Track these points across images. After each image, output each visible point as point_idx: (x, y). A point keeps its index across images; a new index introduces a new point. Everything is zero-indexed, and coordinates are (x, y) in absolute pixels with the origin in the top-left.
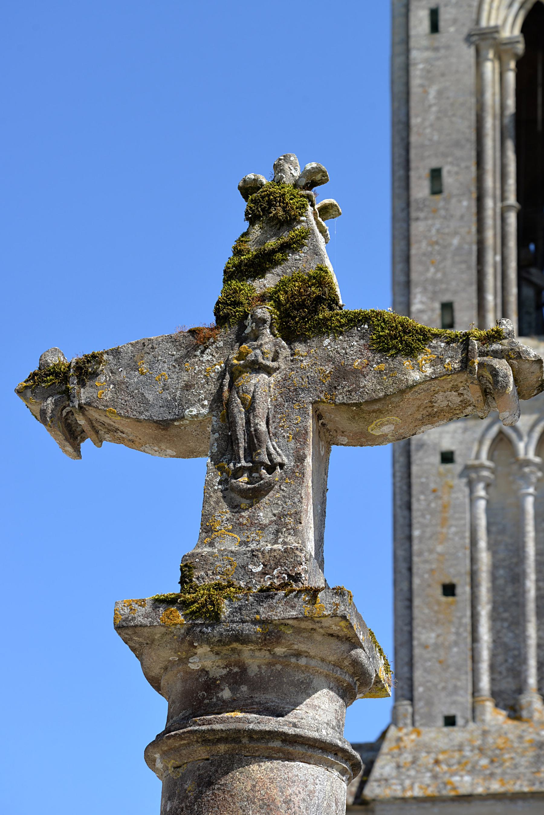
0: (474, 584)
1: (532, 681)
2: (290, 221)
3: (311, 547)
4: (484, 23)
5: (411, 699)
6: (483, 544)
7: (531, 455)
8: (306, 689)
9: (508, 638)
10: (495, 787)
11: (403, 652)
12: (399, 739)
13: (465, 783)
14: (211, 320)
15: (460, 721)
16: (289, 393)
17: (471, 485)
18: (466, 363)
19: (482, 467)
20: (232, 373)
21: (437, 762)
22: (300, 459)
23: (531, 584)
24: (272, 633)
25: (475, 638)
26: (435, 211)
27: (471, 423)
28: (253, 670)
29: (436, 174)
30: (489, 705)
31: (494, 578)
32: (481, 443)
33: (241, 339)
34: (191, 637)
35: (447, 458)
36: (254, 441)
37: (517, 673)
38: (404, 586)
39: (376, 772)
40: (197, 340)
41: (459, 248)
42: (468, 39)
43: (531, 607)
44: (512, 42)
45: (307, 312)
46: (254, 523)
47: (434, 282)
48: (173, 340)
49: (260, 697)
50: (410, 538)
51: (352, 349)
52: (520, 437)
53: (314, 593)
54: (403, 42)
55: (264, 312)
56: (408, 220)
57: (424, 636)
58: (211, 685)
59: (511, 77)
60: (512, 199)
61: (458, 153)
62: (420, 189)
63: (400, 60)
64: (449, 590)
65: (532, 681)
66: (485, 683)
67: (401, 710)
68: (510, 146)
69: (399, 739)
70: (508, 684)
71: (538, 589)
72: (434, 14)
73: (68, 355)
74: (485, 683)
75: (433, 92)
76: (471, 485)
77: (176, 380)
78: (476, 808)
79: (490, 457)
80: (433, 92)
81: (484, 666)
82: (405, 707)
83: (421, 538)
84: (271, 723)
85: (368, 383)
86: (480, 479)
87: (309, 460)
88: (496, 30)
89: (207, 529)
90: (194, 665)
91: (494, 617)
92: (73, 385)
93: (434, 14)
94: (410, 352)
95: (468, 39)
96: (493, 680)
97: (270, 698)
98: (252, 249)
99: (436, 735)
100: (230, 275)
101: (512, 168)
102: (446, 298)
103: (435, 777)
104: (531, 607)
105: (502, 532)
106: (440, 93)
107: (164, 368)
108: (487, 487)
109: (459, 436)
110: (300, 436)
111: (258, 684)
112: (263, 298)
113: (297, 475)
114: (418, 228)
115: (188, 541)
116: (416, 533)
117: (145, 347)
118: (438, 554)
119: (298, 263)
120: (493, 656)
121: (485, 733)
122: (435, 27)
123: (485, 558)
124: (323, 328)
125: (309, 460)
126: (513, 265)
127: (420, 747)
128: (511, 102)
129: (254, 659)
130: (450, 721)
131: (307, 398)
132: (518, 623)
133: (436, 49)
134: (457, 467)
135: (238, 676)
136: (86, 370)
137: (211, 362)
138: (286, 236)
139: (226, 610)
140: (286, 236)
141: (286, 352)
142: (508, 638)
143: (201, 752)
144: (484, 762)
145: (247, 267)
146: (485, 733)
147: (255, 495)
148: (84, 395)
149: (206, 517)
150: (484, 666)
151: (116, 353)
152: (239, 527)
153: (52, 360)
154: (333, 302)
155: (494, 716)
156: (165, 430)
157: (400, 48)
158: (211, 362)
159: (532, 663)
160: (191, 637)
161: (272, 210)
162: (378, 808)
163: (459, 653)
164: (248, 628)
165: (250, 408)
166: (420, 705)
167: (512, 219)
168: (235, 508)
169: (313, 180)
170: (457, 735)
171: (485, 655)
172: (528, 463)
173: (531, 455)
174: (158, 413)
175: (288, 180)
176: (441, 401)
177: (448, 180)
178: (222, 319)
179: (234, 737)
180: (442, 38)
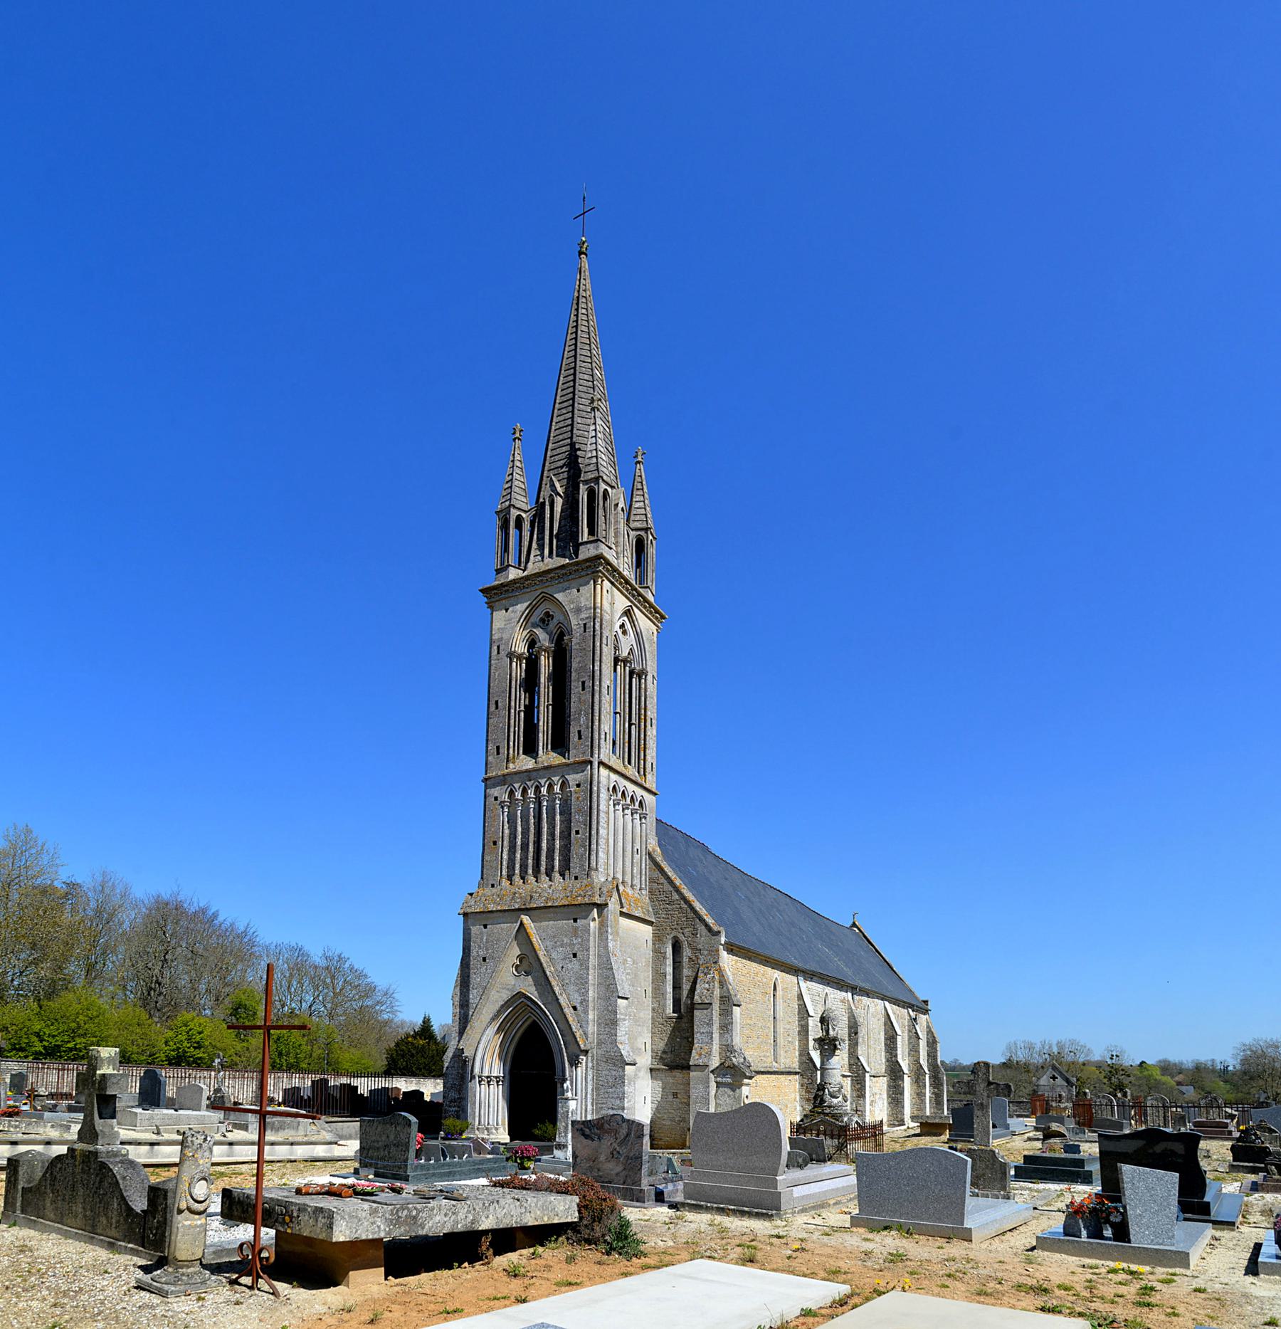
13: (492, 907)
29: (497, 702)
35: (496, 799)
64: (495, 843)
155: (505, 883)
170: (494, 890)
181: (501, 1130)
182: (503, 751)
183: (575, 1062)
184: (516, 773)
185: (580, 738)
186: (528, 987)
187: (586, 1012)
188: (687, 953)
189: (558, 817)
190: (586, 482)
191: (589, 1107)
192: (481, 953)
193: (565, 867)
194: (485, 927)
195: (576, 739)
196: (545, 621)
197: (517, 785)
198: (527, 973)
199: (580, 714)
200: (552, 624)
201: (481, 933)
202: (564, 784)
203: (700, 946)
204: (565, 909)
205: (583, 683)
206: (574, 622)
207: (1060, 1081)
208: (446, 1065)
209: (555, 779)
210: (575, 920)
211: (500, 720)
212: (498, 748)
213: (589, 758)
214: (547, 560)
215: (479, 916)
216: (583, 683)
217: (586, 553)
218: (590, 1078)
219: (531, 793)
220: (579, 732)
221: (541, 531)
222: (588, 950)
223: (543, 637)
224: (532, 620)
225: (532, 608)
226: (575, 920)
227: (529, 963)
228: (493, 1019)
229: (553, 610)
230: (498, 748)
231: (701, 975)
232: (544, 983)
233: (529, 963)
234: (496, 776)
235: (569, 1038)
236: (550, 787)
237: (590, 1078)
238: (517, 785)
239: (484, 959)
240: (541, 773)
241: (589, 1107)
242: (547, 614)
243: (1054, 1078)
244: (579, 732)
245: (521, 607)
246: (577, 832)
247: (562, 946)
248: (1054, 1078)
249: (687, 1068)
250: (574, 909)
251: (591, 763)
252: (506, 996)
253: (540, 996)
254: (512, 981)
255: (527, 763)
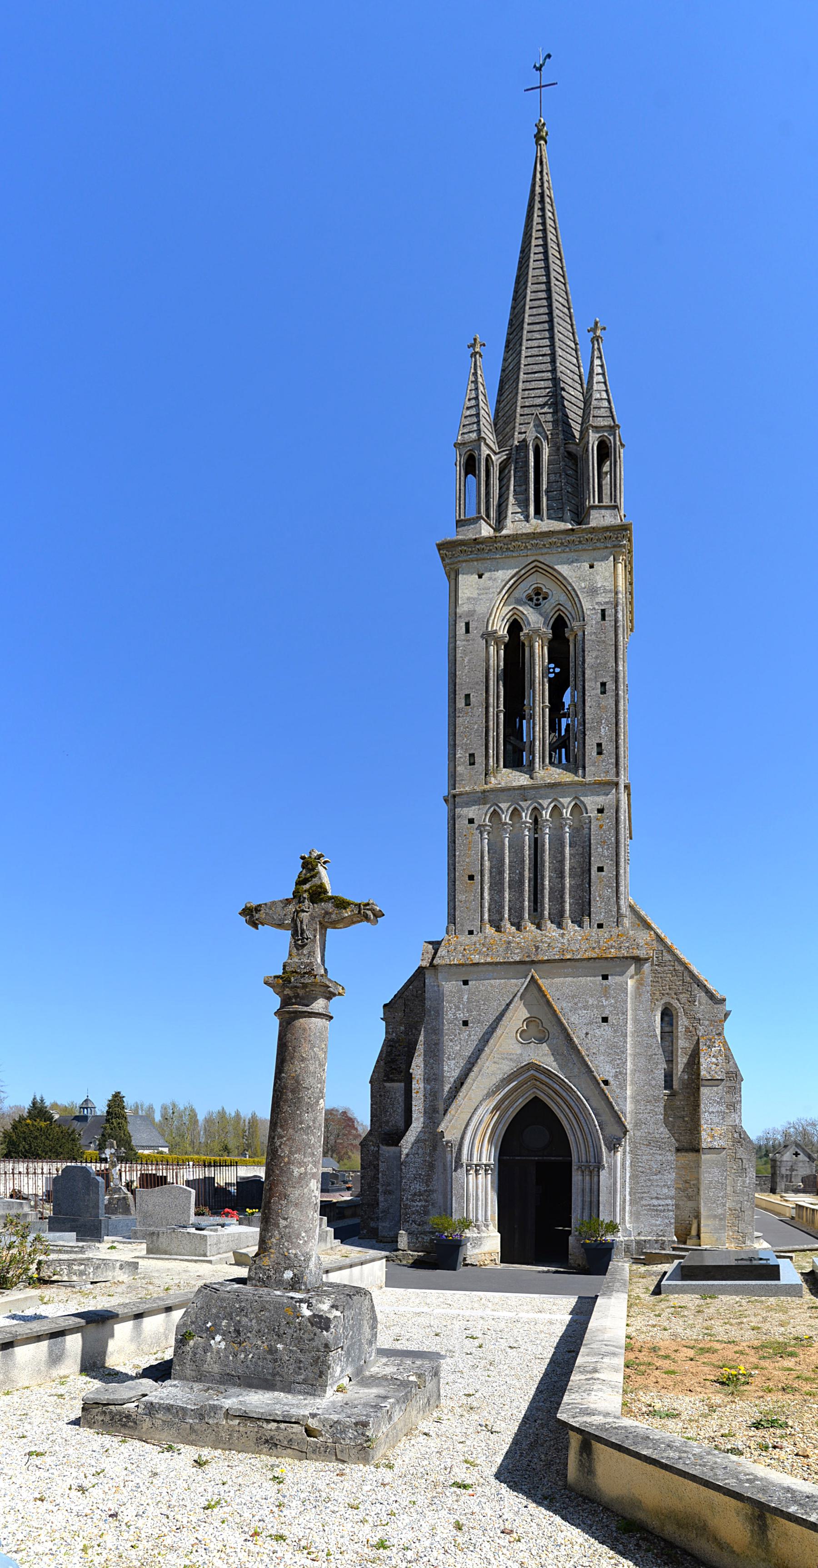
0: (482, 876)
1: (506, 916)
2: (313, 869)
3: (319, 960)
4: (490, 629)
5: (455, 924)
6: (486, 858)
7: (508, 820)
8: (316, 999)
9: (496, 898)
10: (489, 960)
11: (451, 903)
12: (449, 940)
13: (476, 958)
14: (292, 896)
15: (475, 933)
16: (312, 918)
17: (481, 833)
18: (359, 912)
19: (486, 825)
20: (297, 912)
21: (465, 949)
22: (315, 937)
23: (507, 875)
24: (305, 986)
25: (482, 898)
26: (467, 713)
27: (481, 806)
28: (301, 995)
29: (467, 696)
30: (488, 926)
31: (491, 873)
32: (486, 815)
33: (300, 902)
34: (284, 986)
35: (471, 821)
36: (303, 931)
37: (501, 913)
38: (452, 876)
39: (439, 954)
40: (288, 902)
41: (477, 729)
42: (482, 636)
43: (507, 885)
44: (503, 637)
45: (318, 895)
46: (302, 954)
47: (466, 744)
48: (281, 901)
49: (303, 1001)
50: (455, 855)
51: (329, 906)
52: (503, 813)
53: (315, 976)
54: (453, 637)
55: (306, 895)
56: (455, 717)
57: (460, 897)
58: (290, 998)
59: (502, 652)
60: (502, 708)
61: (477, 687)
62: (460, 703)
63: (452, 645)
64: (471, 878)
65: (506, 916)
66: (486, 917)
67: (450, 928)
68: (501, 683)
69: (449, 940)
70: (496, 917)
71: (510, 877)
72: (467, 625)
73: (254, 904)
74: (486, 917)
75: (466, 660)
76: (481, 833)
77: (282, 913)
78: (480, 968)
79: (490, 821)
80: (466, 660)
81: (486, 910)
82: (452, 927)
83: (459, 856)
84: (305, 1009)
85: (333, 916)
86: (485, 831)
87: (318, 937)
88: (496, 632)
89: (290, 955)
90: (285, 993)
91: (490, 889)
92: (254, 913)
93: (467, 625)
94: (345, 908)
95: (482, 636)
96: (489, 915)
97: (306, 1002)
98: (303, 876)
99: (465, 938)
100: (297, 884)
101: (502, 694)
102: (471, 752)
103: (463, 956)
104: (507, 885)
105: (495, 853)
106: (469, 660)
107: (279, 909)
108: (488, 833)
109: (476, 812)
110: (315, 930)
111: (302, 998)
112: (305, 891)
113: (314, 941)
114: (459, 721)
115: (285, 958)
116: (457, 853)
117: (273, 903)
118: (467, 862)
119: (315, 881)
120: (490, 905)
121: (485, 937)
122: (467, 631)
123: (487, 864)
124: (322, 900)
125: (318, 937)
126: (502, 736)
127: (457, 943)
128: (502, 664)
129: (301, 992)
130: (471, 933)
131: (317, 920)
132: (501, 891)
133: (468, 641)
134: (475, 825)
135: (297, 996)
136: (258, 909)
137: (291, 908)
138: (313, 873)
139: (292, 980)
140: (313, 873)
141: (312, 907)
142: (496, 898)
143: (287, 1016)
144: (485, 949)
145: (300, 882)
146: (485, 937)
147: (303, 946)
148: (257, 916)
149: (290, 951)
150: (486, 910)
151: (266, 904)
152: (298, 955)
153: (248, 905)
154: (326, 892)
155: (489, 930)
156: (280, 925)
157: (452, 640)
158: (291, 908)
159: (507, 908)
160: (284, 986)
161: (309, 866)
162: (439, 968)
163: (476, 904)
164: (298, 985)
165: (302, 922)
166: (458, 926)
167: (502, 716)
168: (298, 949)
169: (320, 857)
170: (474, 938)
171: (486, 905)
172: (506, 824)
173: (508, 820)
174: (277, 922)
175: (313, 857)
176: (355, 919)
177: (472, 699)
178: (295, 897)
179: (295, 1012)
180: (470, 636)
181: (491, 1227)
182: (480, 759)
183: (613, 1147)
184: (503, 790)
185: (600, 753)
186: (544, 1056)
187: (623, 1087)
188: (682, 1022)
189: (567, 850)
190: (597, 429)
191: (628, 1198)
192: (461, 1016)
193: (583, 911)
194: (466, 983)
195: (594, 753)
196: (537, 598)
197: (504, 806)
198: (541, 1041)
199: (599, 723)
200: (548, 606)
201: (460, 991)
202: (578, 808)
203: (699, 1016)
204: (591, 964)
205: (603, 685)
206: (586, 605)
207: (802, 1157)
208: (405, 1151)
209: (565, 801)
210: (605, 977)
211: (471, 721)
212: (472, 756)
213: (615, 779)
214: (533, 521)
215: (454, 969)
216: (603, 685)
217: (599, 519)
218: (628, 1163)
219: (526, 817)
220: (599, 745)
221: (523, 481)
222: (625, 1013)
223: (534, 620)
224: (517, 594)
225: (520, 579)
226: (605, 977)
227: (547, 1026)
228: (491, 1094)
229: (547, 585)
230: (472, 756)
231: (702, 1047)
232: (568, 1048)
233: (547, 1026)
234: (474, 792)
235: (607, 1117)
236: (557, 810)
237: (628, 1163)
238: (504, 806)
239: (465, 1023)
240: (542, 792)
241: (628, 1198)
242: (538, 592)
243: (796, 1154)
244: (599, 745)
245: (504, 575)
246: (601, 869)
247: (585, 1008)
248: (796, 1154)
249: (696, 1149)
250: (604, 963)
251: (617, 784)
252: (507, 1067)
253: (561, 1067)
254: (517, 1049)
255: (520, 779)
